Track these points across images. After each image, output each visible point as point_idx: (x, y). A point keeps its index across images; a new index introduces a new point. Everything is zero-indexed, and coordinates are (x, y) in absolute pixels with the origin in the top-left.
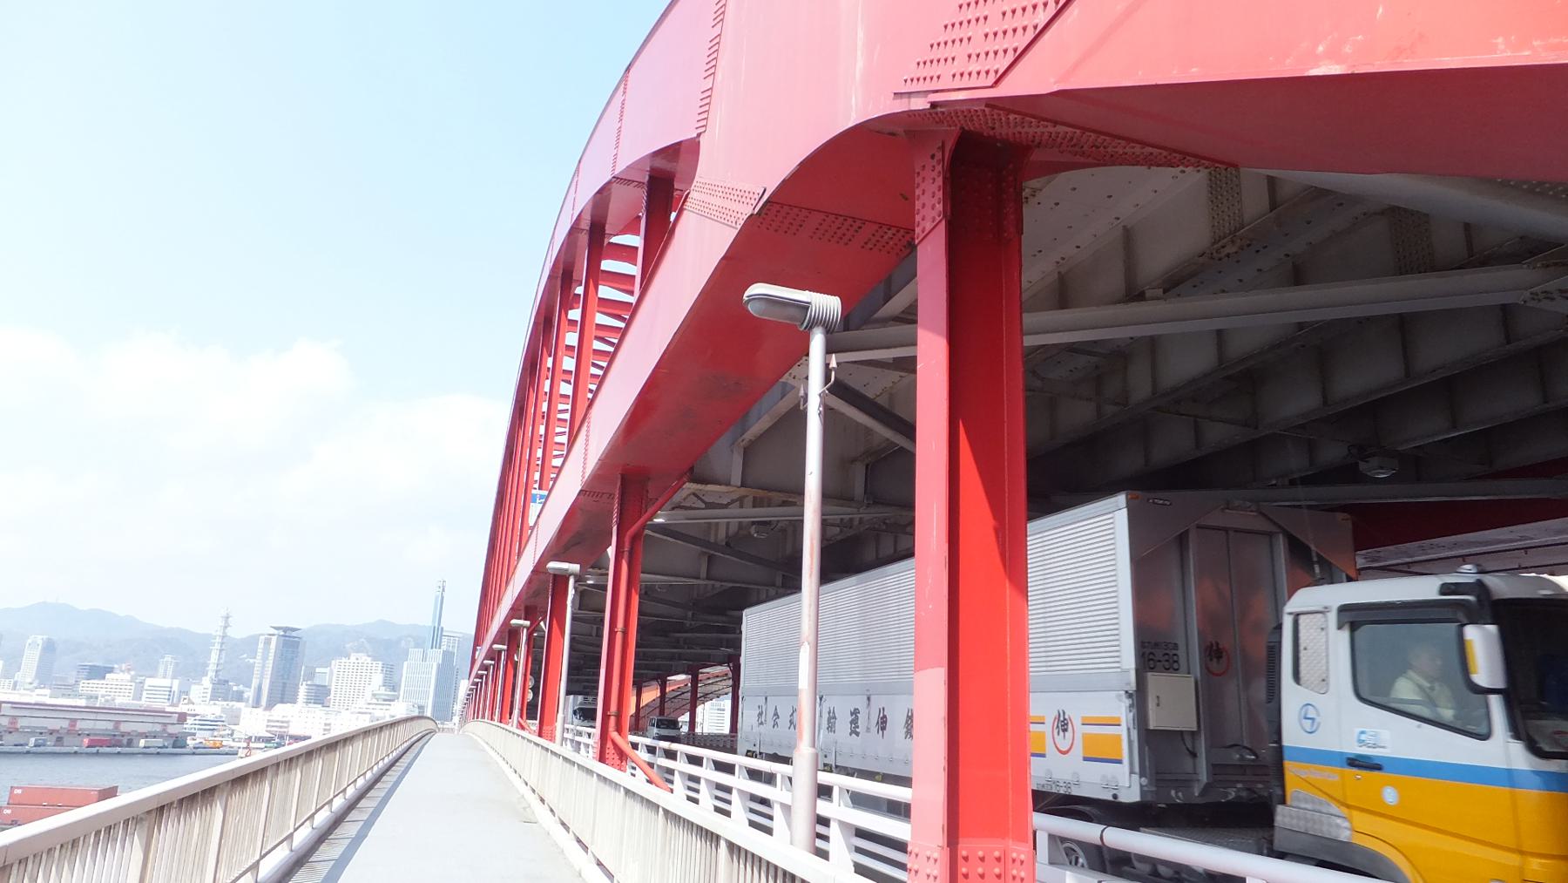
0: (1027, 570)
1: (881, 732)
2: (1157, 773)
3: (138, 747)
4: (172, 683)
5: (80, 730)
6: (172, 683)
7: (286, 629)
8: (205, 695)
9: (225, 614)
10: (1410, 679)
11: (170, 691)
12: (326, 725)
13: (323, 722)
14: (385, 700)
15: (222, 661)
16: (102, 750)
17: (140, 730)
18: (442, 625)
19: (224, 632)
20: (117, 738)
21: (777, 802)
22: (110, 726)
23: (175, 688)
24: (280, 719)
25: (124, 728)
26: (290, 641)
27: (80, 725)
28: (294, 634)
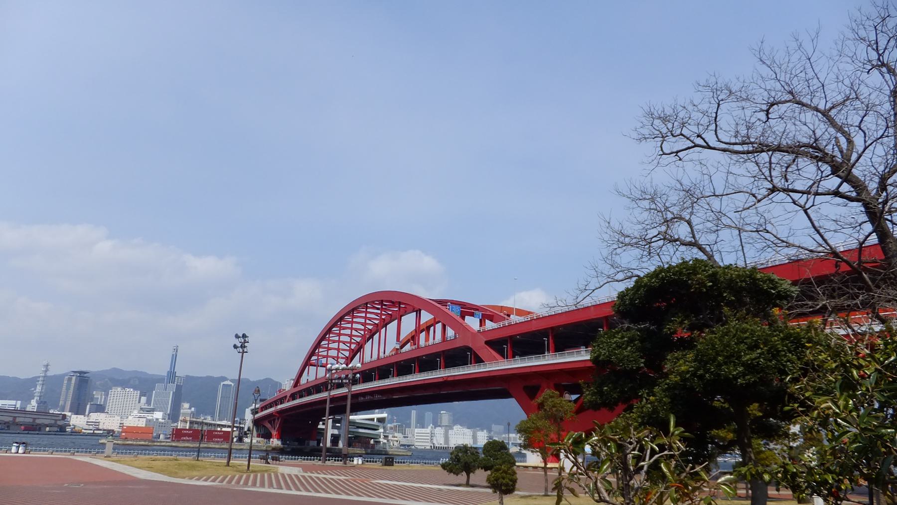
3: (45, 431)
4: (16, 403)
5: (19, 422)
6: (16, 403)
7: (81, 372)
8: (33, 408)
9: (46, 364)
10: (232, 381)
12: (121, 424)
13: (119, 422)
14: (147, 411)
15: (43, 391)
16: (30, 432)
17: (46, 423)
18: (175, 371)
19: (45, 374)
20: (34, 426)
22: (31, 420)
24: (94, 421)
25: (38, 421)
26: (83, 380)
27: (18, 420)
28: (85, 375)
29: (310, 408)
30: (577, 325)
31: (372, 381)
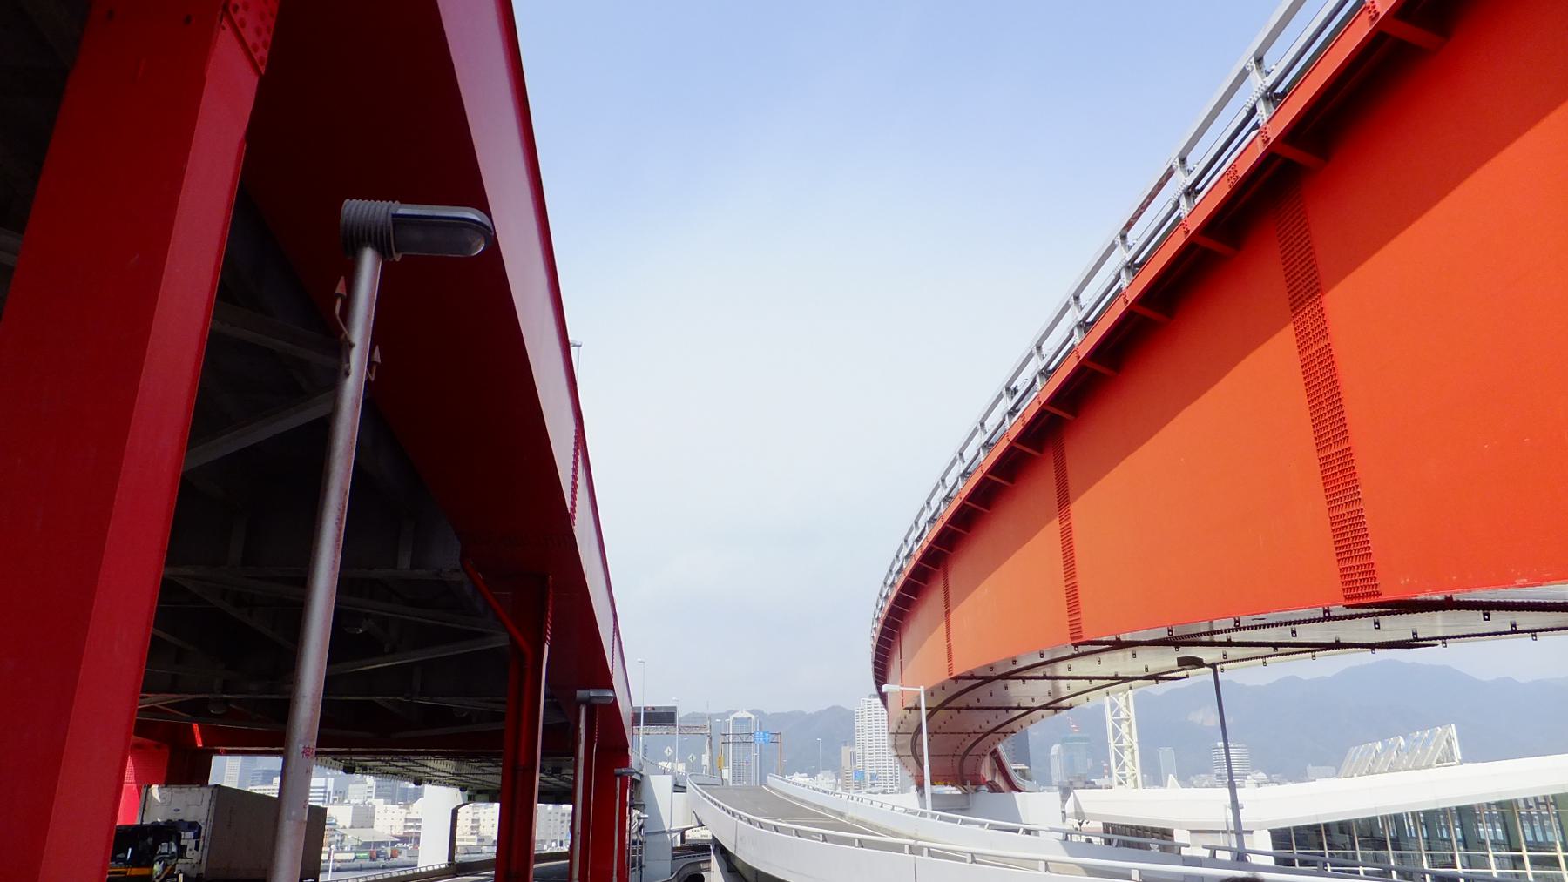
0: (308, 790)
1: (1065, 703)
2: (675, 786)
4: (326, 783)
6: (326, 783)
11: (325, 792)
12: (473, 821)
21: (1181, 825)
23: (330, 788)
26: (1462, 764)
29: (353, 750)
30: (535, 186)
31: (169, 563)
